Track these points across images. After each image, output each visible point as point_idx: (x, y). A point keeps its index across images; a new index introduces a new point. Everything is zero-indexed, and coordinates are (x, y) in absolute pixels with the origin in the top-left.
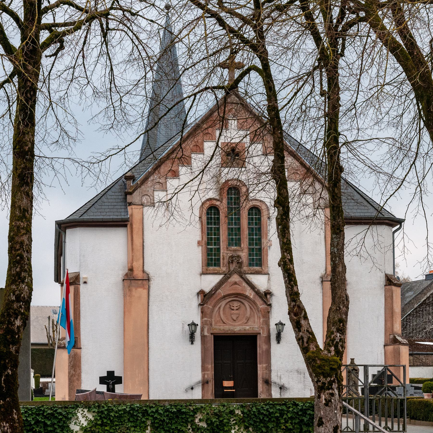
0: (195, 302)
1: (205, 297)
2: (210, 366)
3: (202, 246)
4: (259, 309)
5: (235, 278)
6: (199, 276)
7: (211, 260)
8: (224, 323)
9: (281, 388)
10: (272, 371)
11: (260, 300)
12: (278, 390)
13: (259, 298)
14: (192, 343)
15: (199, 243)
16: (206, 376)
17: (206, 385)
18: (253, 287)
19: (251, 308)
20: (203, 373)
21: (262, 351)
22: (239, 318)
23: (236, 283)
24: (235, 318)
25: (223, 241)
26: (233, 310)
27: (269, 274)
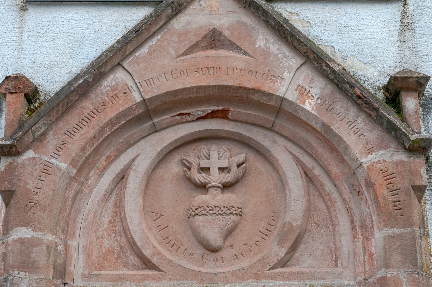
4: (361, 174)
8: (147, 264)
11: (362, 122)
13: (353, 111)
18: (313, 57)
19: (308, 175)
22: (240, 238)
23: (214, 39)
24: (213, 235)
26: (203, 187)
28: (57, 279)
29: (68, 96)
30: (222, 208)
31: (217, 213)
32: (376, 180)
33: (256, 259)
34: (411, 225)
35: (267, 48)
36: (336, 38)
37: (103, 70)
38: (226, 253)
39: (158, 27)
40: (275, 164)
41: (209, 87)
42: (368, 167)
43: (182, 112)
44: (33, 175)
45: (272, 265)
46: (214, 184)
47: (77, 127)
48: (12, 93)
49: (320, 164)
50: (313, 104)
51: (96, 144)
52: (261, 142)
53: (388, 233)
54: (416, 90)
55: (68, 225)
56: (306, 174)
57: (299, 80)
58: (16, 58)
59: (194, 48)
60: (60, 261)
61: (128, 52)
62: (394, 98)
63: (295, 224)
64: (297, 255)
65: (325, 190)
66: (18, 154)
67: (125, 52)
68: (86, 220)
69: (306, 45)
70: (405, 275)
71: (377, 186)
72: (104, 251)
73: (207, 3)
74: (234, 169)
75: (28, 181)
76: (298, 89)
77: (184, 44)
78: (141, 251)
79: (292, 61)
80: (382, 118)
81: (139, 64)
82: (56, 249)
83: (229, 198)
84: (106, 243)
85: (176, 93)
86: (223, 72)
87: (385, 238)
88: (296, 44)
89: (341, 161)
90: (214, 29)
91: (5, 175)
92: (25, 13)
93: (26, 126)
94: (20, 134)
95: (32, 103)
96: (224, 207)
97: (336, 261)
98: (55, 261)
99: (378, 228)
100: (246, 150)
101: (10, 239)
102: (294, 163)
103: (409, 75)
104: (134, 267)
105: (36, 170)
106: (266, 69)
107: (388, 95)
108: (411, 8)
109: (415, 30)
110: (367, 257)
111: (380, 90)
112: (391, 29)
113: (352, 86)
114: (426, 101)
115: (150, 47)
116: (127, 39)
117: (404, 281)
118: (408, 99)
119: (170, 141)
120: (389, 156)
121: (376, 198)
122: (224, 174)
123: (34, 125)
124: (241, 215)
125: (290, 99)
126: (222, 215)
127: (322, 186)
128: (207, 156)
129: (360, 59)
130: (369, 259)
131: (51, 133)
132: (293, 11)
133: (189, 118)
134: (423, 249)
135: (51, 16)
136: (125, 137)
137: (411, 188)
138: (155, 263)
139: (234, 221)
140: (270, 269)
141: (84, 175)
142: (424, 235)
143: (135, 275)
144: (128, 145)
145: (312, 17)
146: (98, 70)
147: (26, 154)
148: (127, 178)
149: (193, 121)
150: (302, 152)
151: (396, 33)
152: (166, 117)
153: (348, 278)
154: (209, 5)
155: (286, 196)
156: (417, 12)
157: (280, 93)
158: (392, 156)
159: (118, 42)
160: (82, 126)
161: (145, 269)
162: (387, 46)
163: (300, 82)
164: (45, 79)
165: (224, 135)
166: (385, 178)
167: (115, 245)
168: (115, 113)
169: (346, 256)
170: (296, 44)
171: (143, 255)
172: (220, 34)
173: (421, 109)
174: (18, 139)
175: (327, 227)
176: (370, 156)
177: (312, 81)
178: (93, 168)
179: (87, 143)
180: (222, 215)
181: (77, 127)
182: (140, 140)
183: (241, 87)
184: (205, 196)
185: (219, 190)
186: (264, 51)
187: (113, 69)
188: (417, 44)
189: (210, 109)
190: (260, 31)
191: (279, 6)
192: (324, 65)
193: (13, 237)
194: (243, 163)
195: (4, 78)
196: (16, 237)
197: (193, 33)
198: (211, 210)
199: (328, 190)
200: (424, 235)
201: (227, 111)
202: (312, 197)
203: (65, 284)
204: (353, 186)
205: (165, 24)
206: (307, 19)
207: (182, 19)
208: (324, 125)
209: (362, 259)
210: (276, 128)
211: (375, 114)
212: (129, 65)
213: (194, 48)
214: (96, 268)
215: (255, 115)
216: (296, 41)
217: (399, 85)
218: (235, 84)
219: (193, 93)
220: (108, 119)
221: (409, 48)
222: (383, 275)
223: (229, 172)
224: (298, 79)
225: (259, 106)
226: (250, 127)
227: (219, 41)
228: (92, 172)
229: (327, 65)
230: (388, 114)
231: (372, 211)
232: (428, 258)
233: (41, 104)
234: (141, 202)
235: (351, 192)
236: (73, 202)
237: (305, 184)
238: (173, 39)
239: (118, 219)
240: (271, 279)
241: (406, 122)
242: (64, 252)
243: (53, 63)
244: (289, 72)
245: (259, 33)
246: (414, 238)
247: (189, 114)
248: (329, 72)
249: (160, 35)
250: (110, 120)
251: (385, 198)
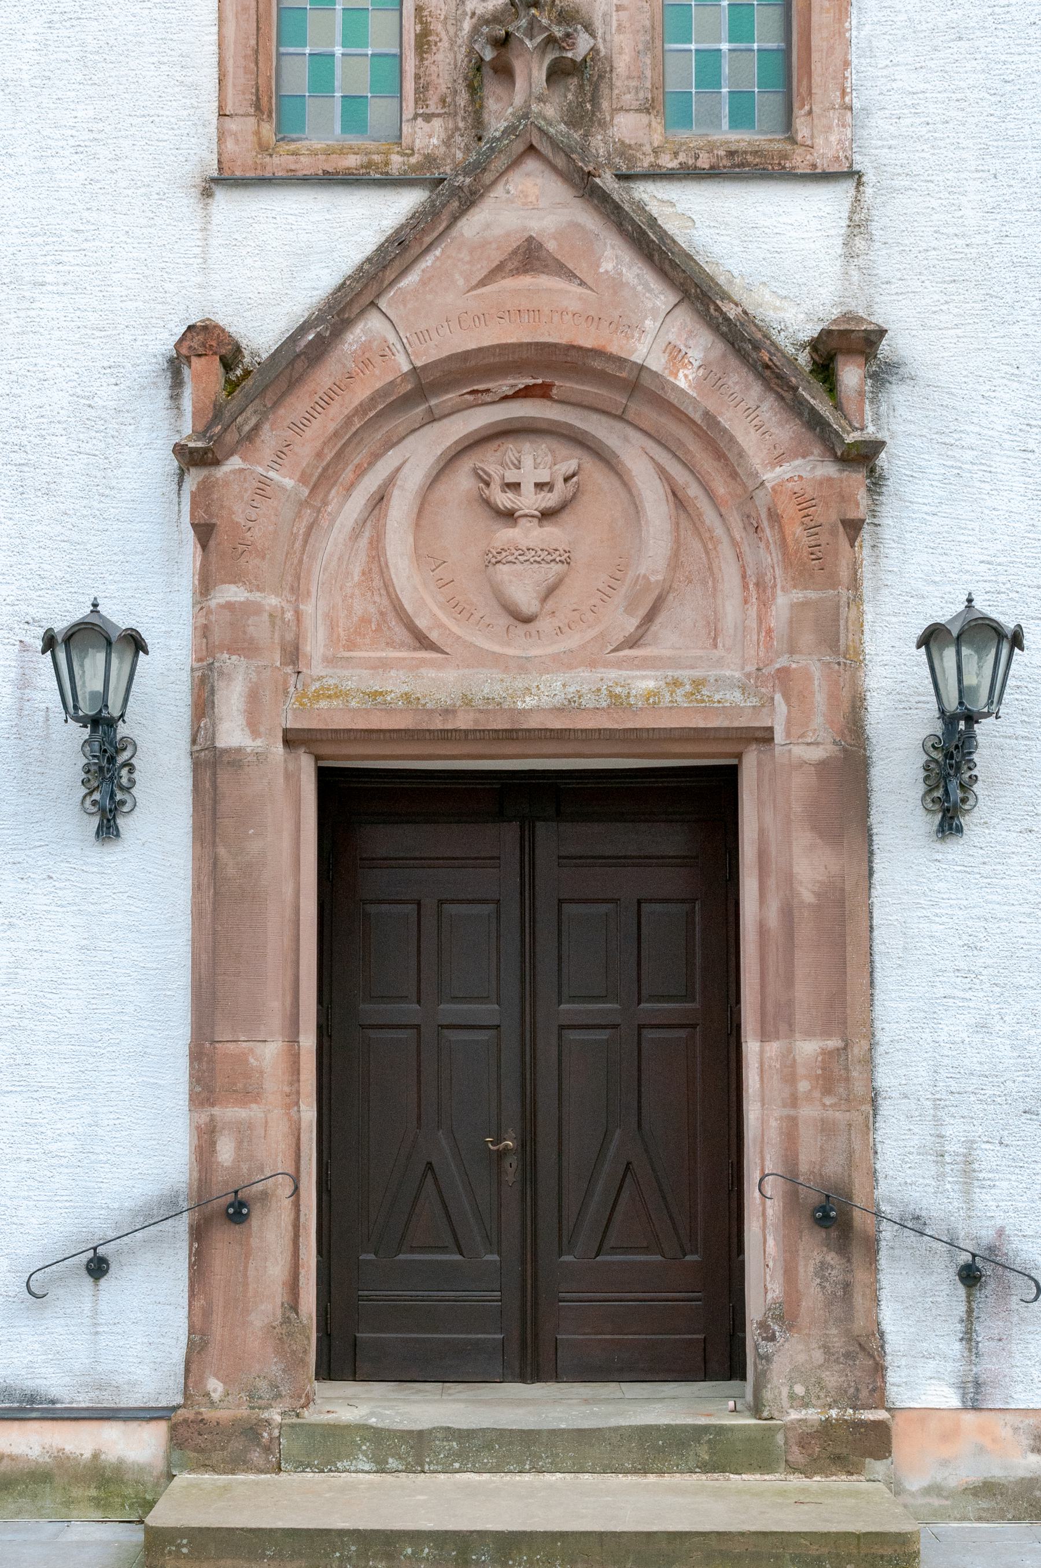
0: (147, 437)
1: (228, 390)
4: (762, 499)
5: (528, 203)
6: (186, 204)
8: (422, 641)
9: (970, 1276)
11: (769, 410)
12: (951, 1296)
13: (756, 389)
14: (108, 828)
16: (226, 1152)
17: (223, 1241)
18: (694, 289)
19: (678, 499)
22: (566, 600)
23: (529, 257)
24: (525, 598)
26: (509, 516)
29: (292, 363)
30: (539, 552)
31: (532, 560)
32: (784, 511)
33: (591, 633)
34: (833, 583)
35: (619, 274)
36: (736, 249)
37: (346, 316)
38: (544, 624)
39: (435, 234)
40: (625, 478)
41: (521, 345)
42: (773, 488)
43: (475, 388)
44: (242, 497)
45: (615, 645)
46: (527, 511)
47: (308, 416)
48: (200, 356)
49: (698, 478)
50: (690, 377)
51: (339, 445)
52: (604, 440)
53: (798, 598)
54: (862, 353)
55: (299, 579)
56: (674, 494)
57: (670, 334)
58: (200, 286)
59: (497, 271)
60: (289, 636)
61: (386, 282)
62: (826, 363)
63: (653, 579)
64: (654, 628)
65: (703, 523)
66: (217, 463)
67: (382, 282)
68: (325, 569)
69: (684, 271)
70: (818, 664)
71: (785, 520)
72: (355, 619)
73: (520, 187)
74: (559, 485)
75: (235, 508)
76: (668, 351)
77: (479, 266)
78: (412, 621)
79: (657, 297)
80: (801, 404)
81: (404, 302)
82: (283, 619)
83: (550, 534)
84: (359, 607)
85: (466, 355)
86: (544, 319)
87: (793, 606)
88: (667, 267)
89: (731, 475)
90: (531, 237)
91: (197, 499)
92: (210, 201)
93: (227, 414)
94: (218, 429)
95: (231, 370)
96: (542, 550)
97: (715, 639)
98: (282, 638)
99: (783, 589)
100: (578, 452)
101: (213, 603)
102: (656, 477)
103: (852, 326)
104: (403, 645)
105: (246, 490)
106: (616, 314)
107: (817, 358)
108: (868, 190)
109: (872, 234)
110: (764, 634)
111: (805, 348)
112: (832, 232)
113: (757, 348)
114: (880, 367)
115: (423, 271)
116: (384, 258)
117: (817, 674)
118: (847, 369)
119: (457, 438)
120: (808, 469)
121: (783, 539)
122: (543, 494)
123: (240, 414)
124: (568, 563)
125: (654, 369)
126: (539, 563)
127: (700, 515)
128: (516, 462)
129: (775, 289)
130: (765, 637)
131: (266, 427)
132: (666, 198)
133: (488, 398)
134: (850, 623)
135: (254, 208)
136: (386, 429)
137: (840, 525)
138: (434, 640)
139: (558, 574)
140: (613, 651)
141: (321, 496)
142: (854, 600)
143: (404, 659)
144: (390, 444)
145: (698, 208)
146: (338, 315)
147: (228, 462)
148: (389, 501)
149: (493, 403)
150: (670, 456)
151: (840, 241)
152: (451, 397)
153: (732, 666)
154: (522, 192)
155: (640, 530)
156: (878, 200)
157: (637, 358)
158: (814, 468)
159: (369, 260)
160: (316, 414)
161: (420, 649)
162: (821, 265)
163: (671, 337)
164: (250, 326)
165: (544, 426)
166: (799, 507)
167: (372, 609)
168: (368, 393)
169: (731, 631)
170: (667, 267)
171: (416, 627)
172: (540, 246)
173: (869, 382)
174: (215, 438)
175: (704, 582)
176: (778, 469)
177: (691, 334)
178: (333, 485)
179: (325, 443)
180: (539, 563)
181: (308, 416)
182: (407, 435)
183: (573, 347)
184: (511, 530)
185: (536, 521)
186: (614, 279)
187: (362, 312)
188: (874, 262)
189: (523, 382)
190: (608, 242)
191: (642, 188)
192: (712, 308)
193: (217, 601)
195: (185, 328)
196: (222, 601)
197: (494, 246)
198: (521, 554)
199: (708, 522)
200: (854, 600)
201: (550, 386)
202: (682, 533)
203: (299, 673)
204: (748, 517)
205: (448, 227)
206: (689, 213)
207: (476, 218)
208: (707, 414)
209: (755, 637)
210: (630, 415)
211: (791, 397)
212: (389, 305)
213: (497, 271)
214: (344, 646)
215: (596, 394)
216: (667, 262)
217: (834, 344)
218: (564, 341)
219: (494, 355)
220: (356, 402)
221: (860, 268)
222: (786, 664)
223: (551, 490)
224: (668, 332)
225: (603, 378)
226: (586, 412)
227: (538, 259)
228: (333, 492)
229: (718, 309)
230: (813, 397)
231: (775, 560)
232: (856, 637)
233: (247, 373)
234: (411, 539)
235: (745, 528)
236: (306, 542)
237: (673, 512)
239: (375, 568)
240: (613, 666)
241: (841, 410)
242: (295, 622)
243: (262, 296)
244: (654, 320)
245: (605, 244)
246: (838, 607)
247: (488, 391)
248: (720, 320)
249: (440, 249)
250: (361, 405)
251: (797, 541)
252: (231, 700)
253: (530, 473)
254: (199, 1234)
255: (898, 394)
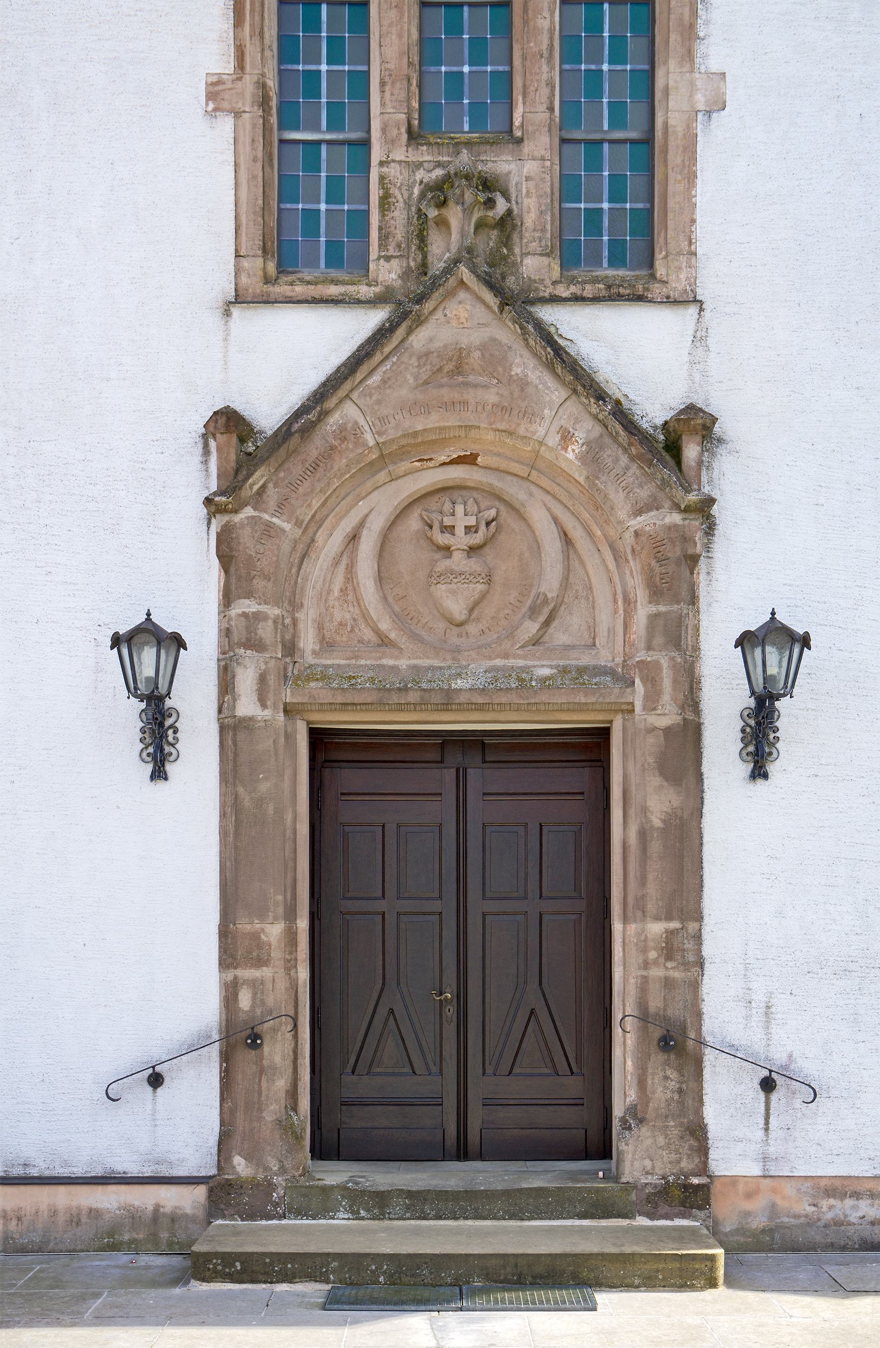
0: (191, 480)
1: (241, 449)
2: (285, 932)
3: (237, 115)
5: (463, 320)
6: (214, 320)
7: (293, 240)
9: (768, 1085)
10: (705, 1017)
14: (159, 774)
15: (215, 93)
16: (245, 1000)
19: (567, 540)
20: (230, 976)
21: (643, 835)
23: (454, 366)
25: (383, 84)
26: (447, 550)
27: (695, 301)
28: (286, 656)
47: (301, 478)
55: (295, 595)
60: (288, 637)
63: (549, 596)
78: (377, 626)
81: (371, 395)
82: (283, 624)
92: (229, 319)
98: (283, 637)
105: (256, 531)
133: (431, 464)
148: (360, 538)
152: (405, 466)
160: (306, 477)
163: (563, 422)
171: (379, 629)
181: (301, 478)
194: (493, 520)
197: (435, 354)
207: (422, 334)
236: (300, 568)
238: (412, 362)
239: (350, 588)
247: (431, 459)
252: (246, 680)
253: (461, 521)
254: (226, 1057)
255: (722, 450)
